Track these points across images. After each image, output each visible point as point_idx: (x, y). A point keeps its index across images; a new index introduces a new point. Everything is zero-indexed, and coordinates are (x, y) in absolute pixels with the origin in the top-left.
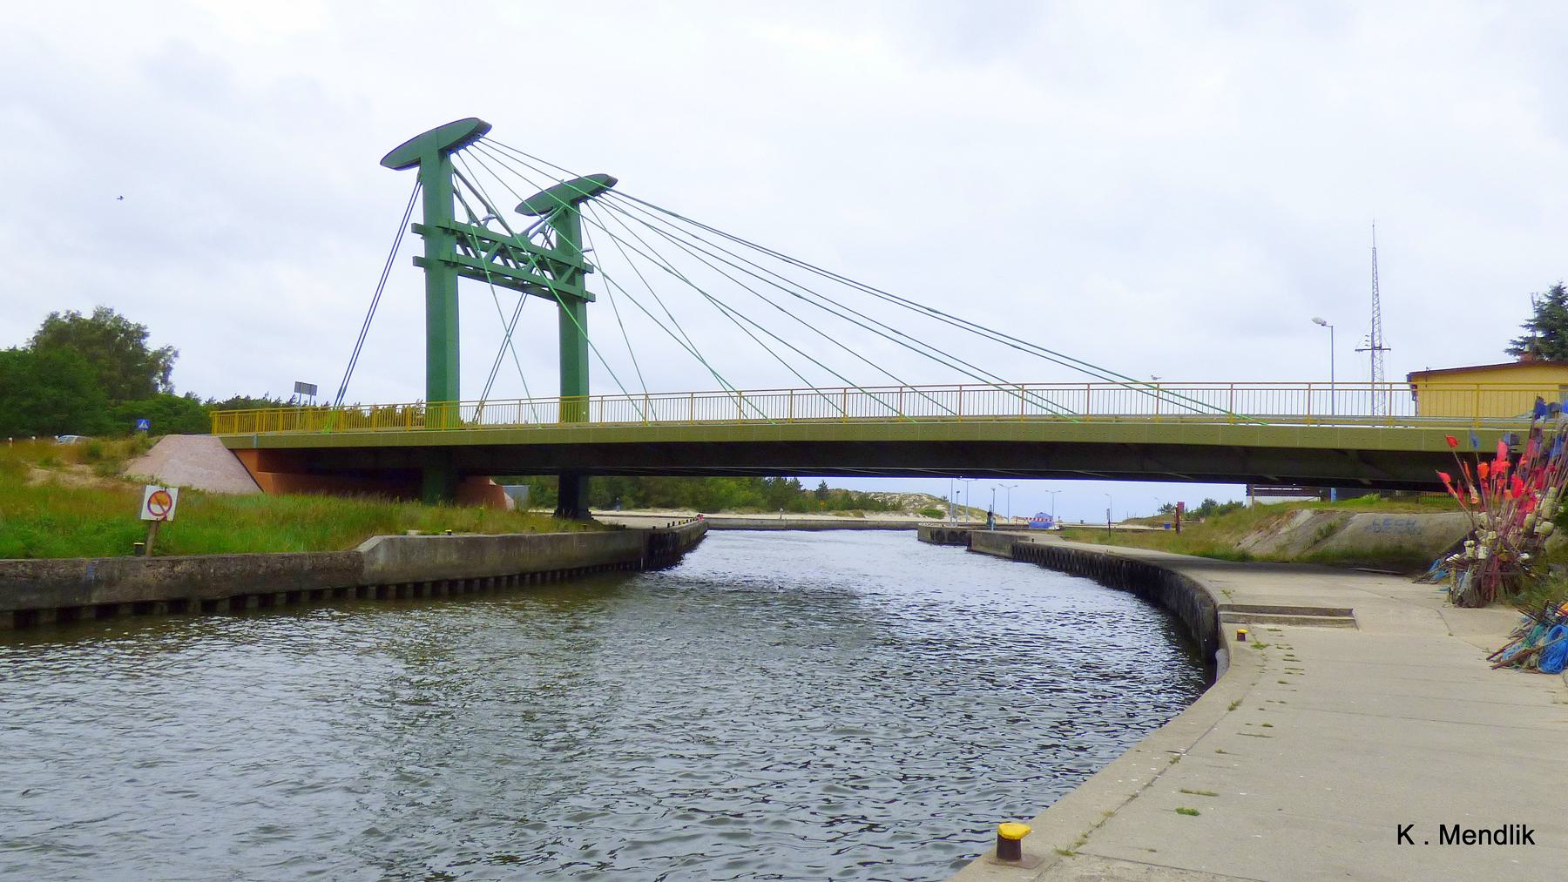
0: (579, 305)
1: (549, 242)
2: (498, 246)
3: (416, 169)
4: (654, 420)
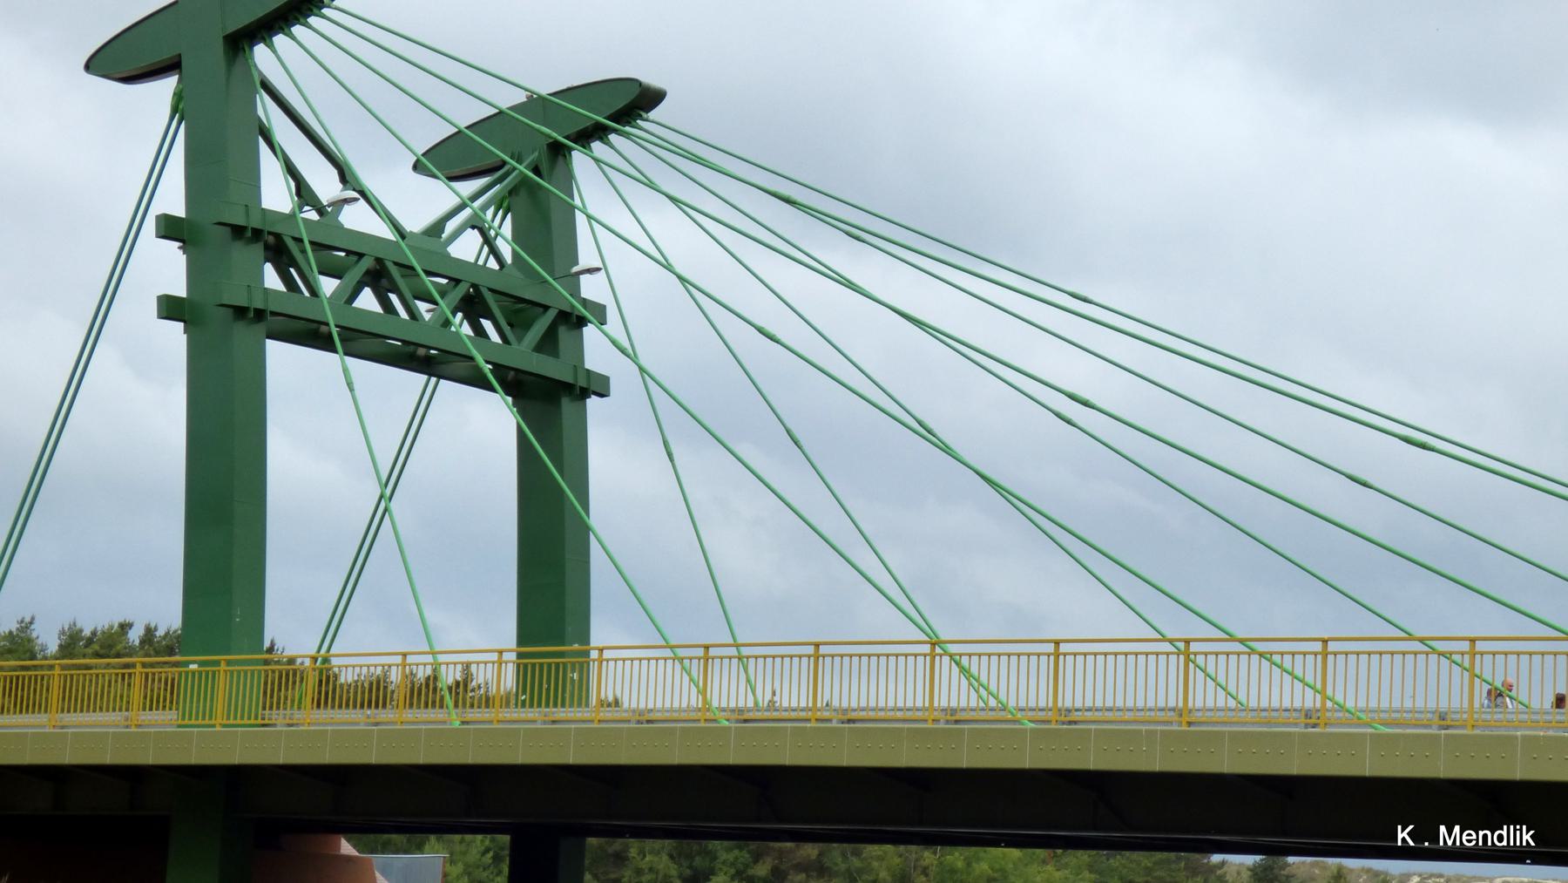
0: (567, 405)
1: (494, 251)
2: (367, 263)
3: (167, 86)
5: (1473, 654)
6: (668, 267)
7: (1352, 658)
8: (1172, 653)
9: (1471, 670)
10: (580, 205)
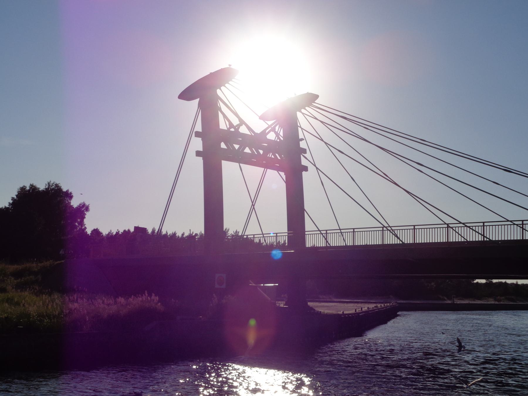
4: (344, 245)
5: (341, 233)
6: (322, 140)
7: (436, 229)
8: (386, 230)
9: (522, 228)
10: (299, 126)
